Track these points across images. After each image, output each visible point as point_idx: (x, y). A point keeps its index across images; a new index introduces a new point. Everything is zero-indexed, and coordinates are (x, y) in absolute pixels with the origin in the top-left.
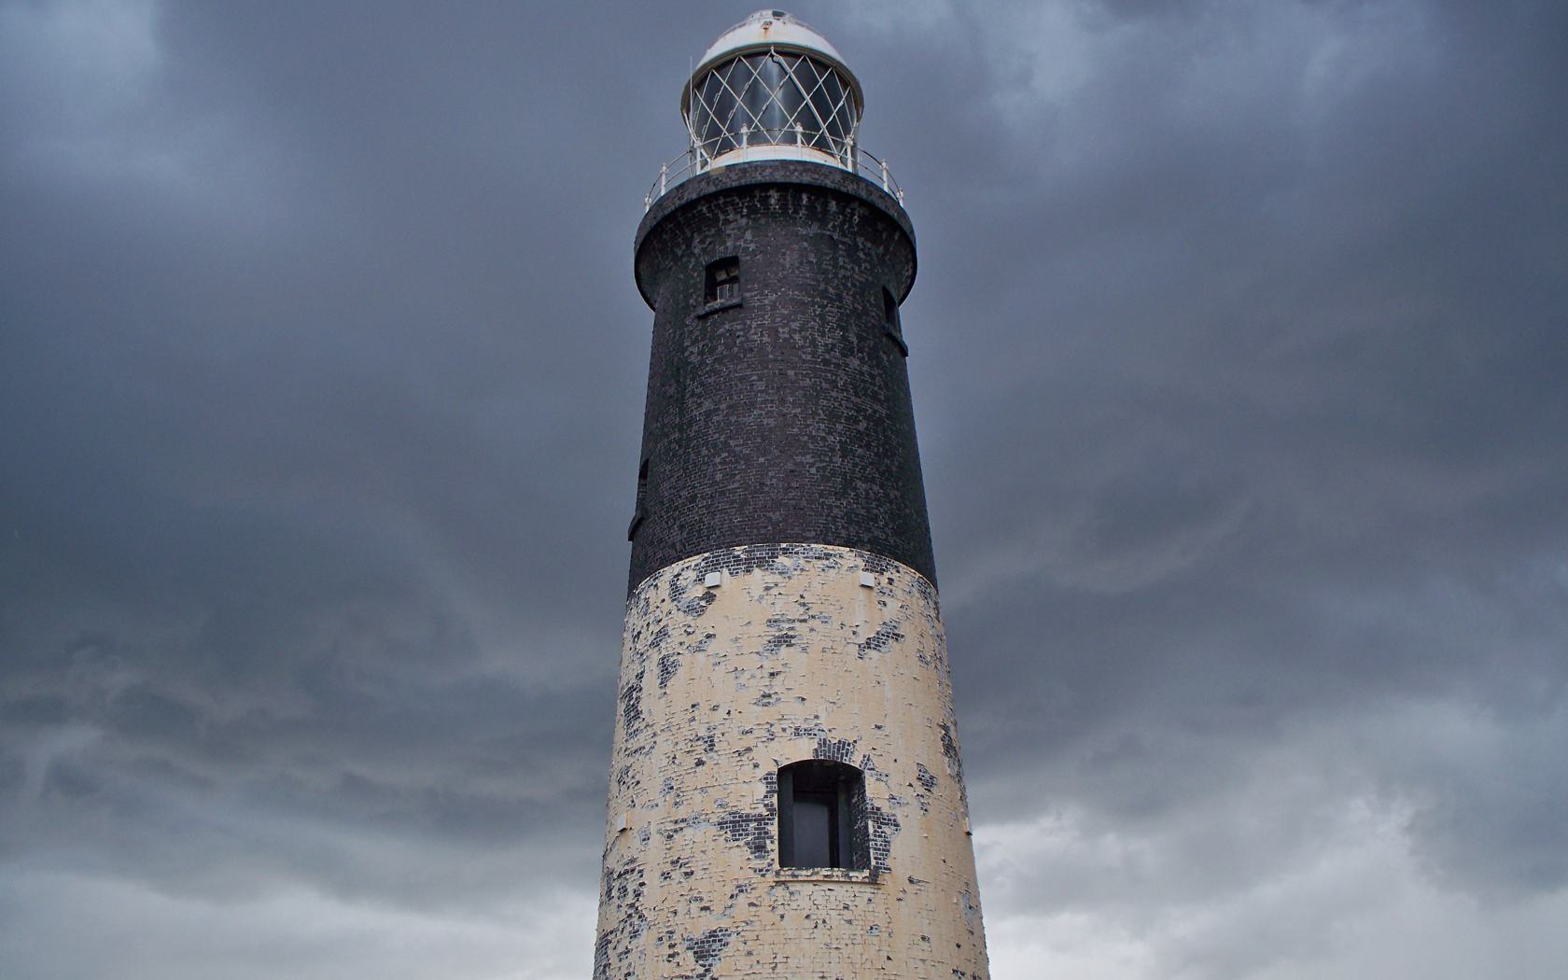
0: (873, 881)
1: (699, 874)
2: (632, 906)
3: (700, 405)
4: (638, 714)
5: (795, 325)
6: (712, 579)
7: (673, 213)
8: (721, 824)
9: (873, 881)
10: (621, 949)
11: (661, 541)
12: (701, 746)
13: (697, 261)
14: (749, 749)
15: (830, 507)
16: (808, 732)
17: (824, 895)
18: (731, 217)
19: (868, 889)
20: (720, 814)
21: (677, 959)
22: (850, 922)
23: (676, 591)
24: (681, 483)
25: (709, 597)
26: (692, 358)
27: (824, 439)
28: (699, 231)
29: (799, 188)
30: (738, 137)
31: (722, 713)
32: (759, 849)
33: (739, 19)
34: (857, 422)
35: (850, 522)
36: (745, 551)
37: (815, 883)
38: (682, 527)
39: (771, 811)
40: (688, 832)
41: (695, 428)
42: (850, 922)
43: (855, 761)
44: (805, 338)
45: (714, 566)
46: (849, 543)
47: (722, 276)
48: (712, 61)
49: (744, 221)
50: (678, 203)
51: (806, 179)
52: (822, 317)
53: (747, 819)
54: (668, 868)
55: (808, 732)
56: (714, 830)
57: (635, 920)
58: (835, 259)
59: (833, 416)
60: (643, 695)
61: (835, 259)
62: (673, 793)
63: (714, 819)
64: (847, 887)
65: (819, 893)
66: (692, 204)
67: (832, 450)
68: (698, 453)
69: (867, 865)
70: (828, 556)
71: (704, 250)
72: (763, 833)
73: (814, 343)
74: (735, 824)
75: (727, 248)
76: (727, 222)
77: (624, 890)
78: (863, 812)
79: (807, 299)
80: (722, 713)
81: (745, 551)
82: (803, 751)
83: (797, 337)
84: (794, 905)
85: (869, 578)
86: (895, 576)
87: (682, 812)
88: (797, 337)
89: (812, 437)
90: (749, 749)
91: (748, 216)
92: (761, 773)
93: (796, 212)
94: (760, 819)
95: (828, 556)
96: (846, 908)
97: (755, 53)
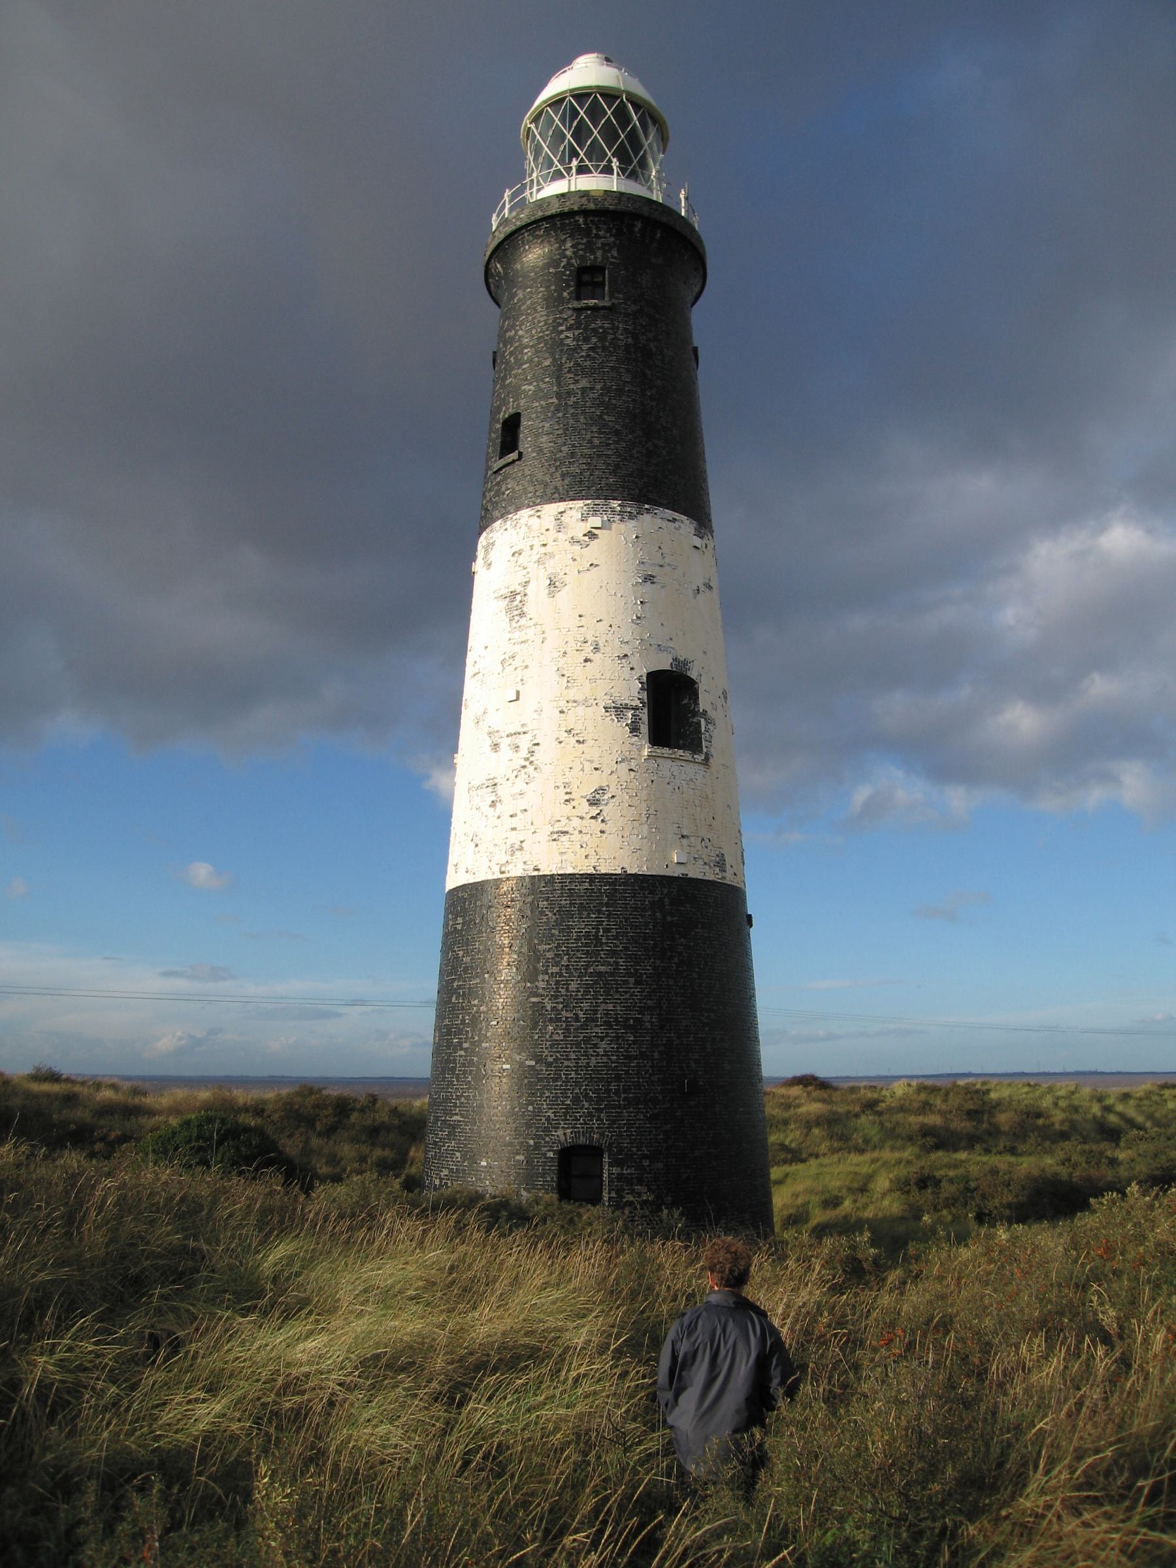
7: (552, 217)
9: (706, 761)
12: (589, 648)
19: (702, 767)
21: (573, 803)
30: (569, 170)
37: (673, 759)
43: (693, 675)
47: (586, 278)
48: (545, 102)
51: (664, 219)
53: (626, 707)
54: (563, 736)
57: (530, 769)
64: (691, 765)
65: (675, 767)
69: (701, 751)
76: (597, 236)
82: (665, 664)
83: (652, 345)
85: (697, 541)
88: (652, 345)
95: (674, 520)
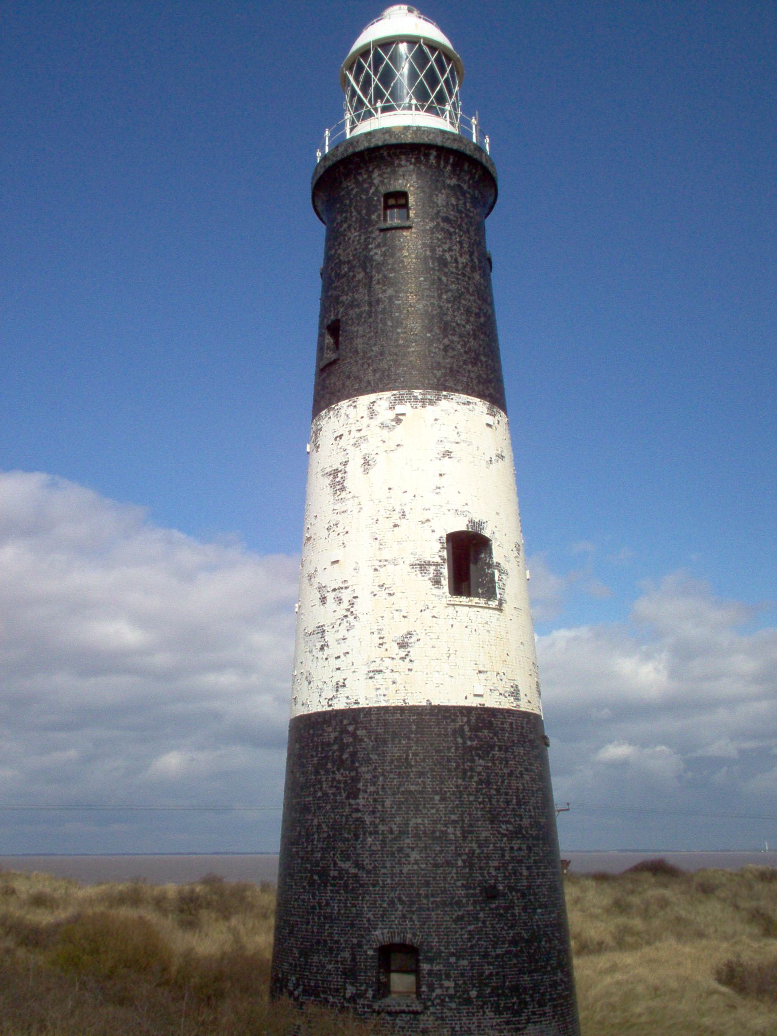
0: (500, 608)
1: (398, 595)
2: (348, 610)
3: (385, 291)
4: (343, 489)
5: (446, 247)
6: (400, 409)
8: (412, 566)
9: (500, 608)
10: (340, 636)
11: (357, 378)
13: (377, 189)
14: (428, 520)
15: (469, 372)
16: (462, 513)
17: (470, 612)
18: (403, 163)
19: (496, 612)
20: (413, 560)
21: (385, 646)
22: (488, 631)
23: (372, 414)
24: (372, 342)
25: (398, 420)
26: (377, 257)
27: (464, 326)
28: (378, 167)
29: (450, 151)
31: (351, 495)
32: (437, 582)
33: (375, 13)
34: (480, 317)
35: (479, 382)
36: (421, 394)
37: (470, 606)
38: (375, 371)
39: (443, 560)
40: (390, 567)
41: (381, 306)
42: (488, 631)
43: (487, 533)
44: (452, 257)
45: (400, 400)
46: (481, 396)
47: (392, 202)
49: (412, 167)
50: (366, 145)
51: (455, 146)
52: (460, 243)
53: (429, 564)
55: (462, 513)
56: (409, 569)
57: (351, 618)
58: (465, 203)
59: (468, 311)
60: (349, 476)
61: (465, 203)
62: (378, 541)
63: (408, 562)
64: (486, 610)
66: (378, 148)
67: (469, 334)
68: (385, 324)
69: (495, 598)
70: (469, 403)
71: (382, 182)
72: (438, 574)
73: (456, 261)
74: (423, 566)
75: (399, 184)
77: (340, 601)
78: (490, 566)
79: (452, 230)
80: (409, 496)
81: (421, 394)
82: (461, 526)
84: (459, 619)
86: (500, 419)
87: (386, 554)
89: (458, 325)
90: (428, 520)
91: (415, 164)
92: (437, 536)
93: (445, 167)
94: (437, 564)
95: (469, 403)
96: (487, 623)
97: (387, 44)
